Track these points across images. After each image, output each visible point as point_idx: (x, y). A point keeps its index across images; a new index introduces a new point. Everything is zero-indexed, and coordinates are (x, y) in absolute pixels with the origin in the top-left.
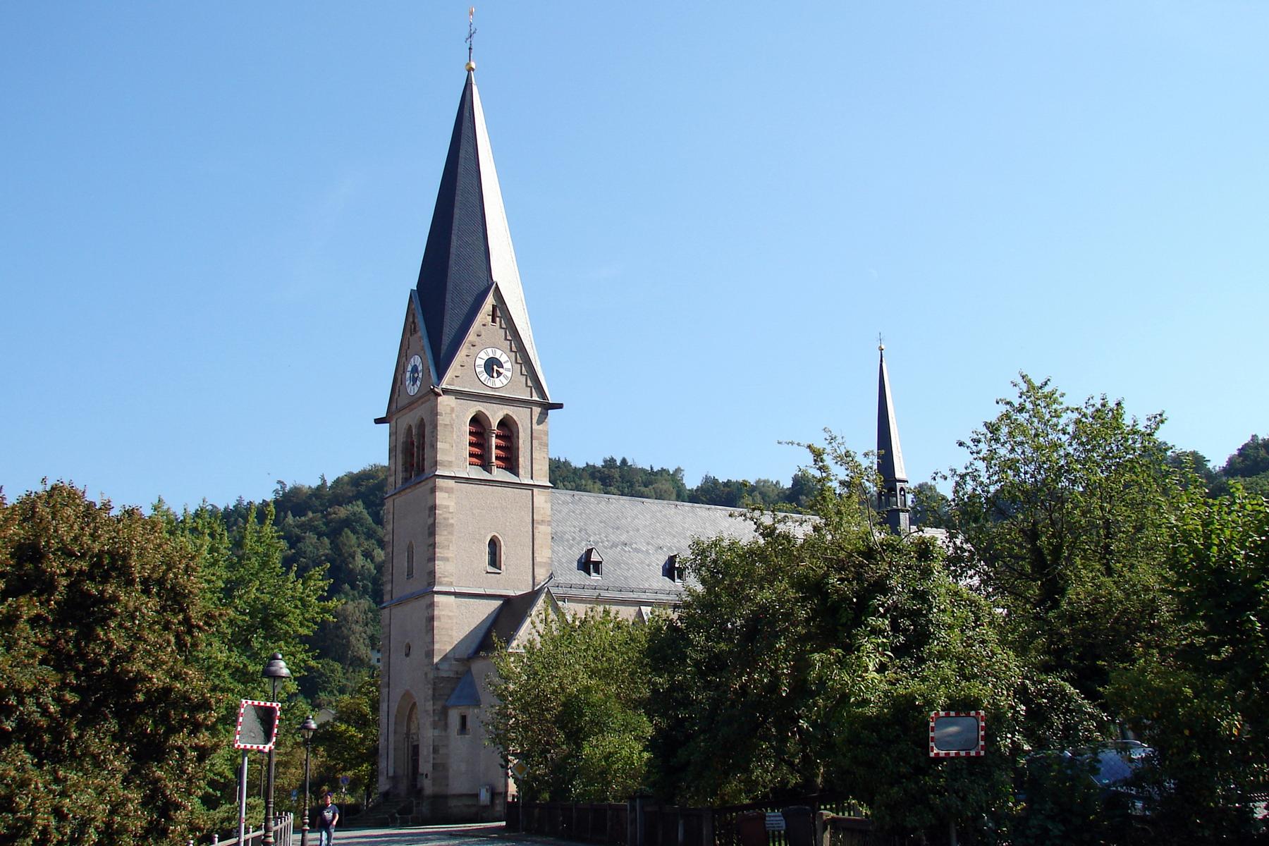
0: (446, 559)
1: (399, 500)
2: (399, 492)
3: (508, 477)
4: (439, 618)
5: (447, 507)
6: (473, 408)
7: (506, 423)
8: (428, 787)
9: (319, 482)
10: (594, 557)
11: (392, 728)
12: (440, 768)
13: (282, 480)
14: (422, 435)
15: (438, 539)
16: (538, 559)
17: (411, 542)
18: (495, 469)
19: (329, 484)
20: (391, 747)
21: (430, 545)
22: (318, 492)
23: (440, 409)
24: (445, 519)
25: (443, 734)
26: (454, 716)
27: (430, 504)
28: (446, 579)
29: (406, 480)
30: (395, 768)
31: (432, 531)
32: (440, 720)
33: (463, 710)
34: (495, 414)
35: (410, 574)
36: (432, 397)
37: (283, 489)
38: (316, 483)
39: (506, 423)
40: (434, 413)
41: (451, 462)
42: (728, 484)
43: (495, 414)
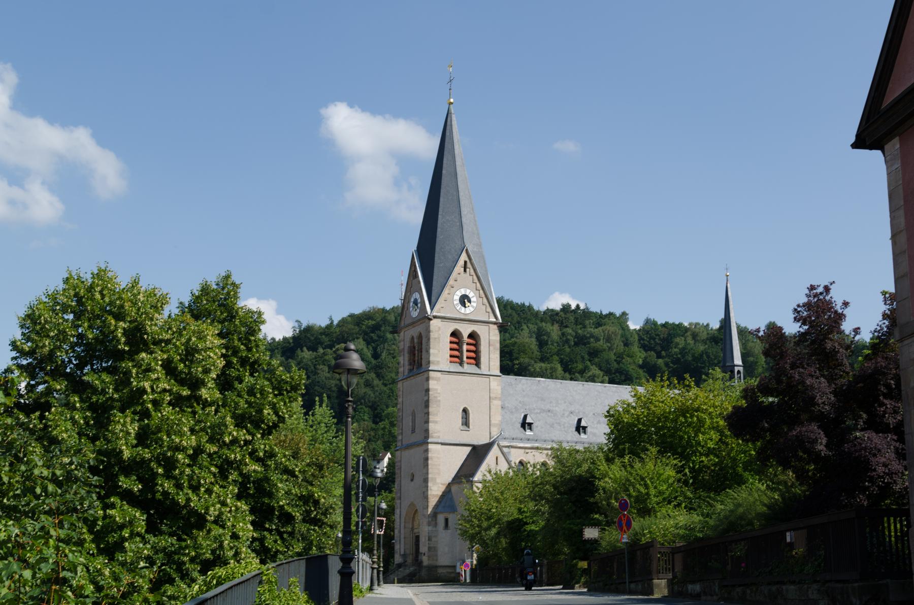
0: (436, 422)
1: (407, 383)
2: (406, 378)
3: (473, 369)
4: (432, 458)
5: (437, 390)
6: (453, 326)
7: (473, 335)
8: (425, 561)
9: (328, 322)
10: (529, 420)
11: (402, 525)
12: (432, 549)
13: (300, 320)
14: (421, 343)
15: (431, 410)
16: (493, 422)
17: (414, 410)
18: (465, 365)
19: (335, 323)
20: (402, 536)
21: (426, 413)
22: (327, 331)
23: (432, 328)
24: (435, 397)
25: (434, 529)
27: (425, 388)
28: (436, 434)
29: (410, 370)
30: (405, 550)
31: (427, 405)
32: (432, 520)
35: (413, 431)
36: (427, 321)
37: (300, 327)
38: (324, 323)
39: (473, 335)
40: (428, 331)
41: (438, 362)
42: (665, 325)
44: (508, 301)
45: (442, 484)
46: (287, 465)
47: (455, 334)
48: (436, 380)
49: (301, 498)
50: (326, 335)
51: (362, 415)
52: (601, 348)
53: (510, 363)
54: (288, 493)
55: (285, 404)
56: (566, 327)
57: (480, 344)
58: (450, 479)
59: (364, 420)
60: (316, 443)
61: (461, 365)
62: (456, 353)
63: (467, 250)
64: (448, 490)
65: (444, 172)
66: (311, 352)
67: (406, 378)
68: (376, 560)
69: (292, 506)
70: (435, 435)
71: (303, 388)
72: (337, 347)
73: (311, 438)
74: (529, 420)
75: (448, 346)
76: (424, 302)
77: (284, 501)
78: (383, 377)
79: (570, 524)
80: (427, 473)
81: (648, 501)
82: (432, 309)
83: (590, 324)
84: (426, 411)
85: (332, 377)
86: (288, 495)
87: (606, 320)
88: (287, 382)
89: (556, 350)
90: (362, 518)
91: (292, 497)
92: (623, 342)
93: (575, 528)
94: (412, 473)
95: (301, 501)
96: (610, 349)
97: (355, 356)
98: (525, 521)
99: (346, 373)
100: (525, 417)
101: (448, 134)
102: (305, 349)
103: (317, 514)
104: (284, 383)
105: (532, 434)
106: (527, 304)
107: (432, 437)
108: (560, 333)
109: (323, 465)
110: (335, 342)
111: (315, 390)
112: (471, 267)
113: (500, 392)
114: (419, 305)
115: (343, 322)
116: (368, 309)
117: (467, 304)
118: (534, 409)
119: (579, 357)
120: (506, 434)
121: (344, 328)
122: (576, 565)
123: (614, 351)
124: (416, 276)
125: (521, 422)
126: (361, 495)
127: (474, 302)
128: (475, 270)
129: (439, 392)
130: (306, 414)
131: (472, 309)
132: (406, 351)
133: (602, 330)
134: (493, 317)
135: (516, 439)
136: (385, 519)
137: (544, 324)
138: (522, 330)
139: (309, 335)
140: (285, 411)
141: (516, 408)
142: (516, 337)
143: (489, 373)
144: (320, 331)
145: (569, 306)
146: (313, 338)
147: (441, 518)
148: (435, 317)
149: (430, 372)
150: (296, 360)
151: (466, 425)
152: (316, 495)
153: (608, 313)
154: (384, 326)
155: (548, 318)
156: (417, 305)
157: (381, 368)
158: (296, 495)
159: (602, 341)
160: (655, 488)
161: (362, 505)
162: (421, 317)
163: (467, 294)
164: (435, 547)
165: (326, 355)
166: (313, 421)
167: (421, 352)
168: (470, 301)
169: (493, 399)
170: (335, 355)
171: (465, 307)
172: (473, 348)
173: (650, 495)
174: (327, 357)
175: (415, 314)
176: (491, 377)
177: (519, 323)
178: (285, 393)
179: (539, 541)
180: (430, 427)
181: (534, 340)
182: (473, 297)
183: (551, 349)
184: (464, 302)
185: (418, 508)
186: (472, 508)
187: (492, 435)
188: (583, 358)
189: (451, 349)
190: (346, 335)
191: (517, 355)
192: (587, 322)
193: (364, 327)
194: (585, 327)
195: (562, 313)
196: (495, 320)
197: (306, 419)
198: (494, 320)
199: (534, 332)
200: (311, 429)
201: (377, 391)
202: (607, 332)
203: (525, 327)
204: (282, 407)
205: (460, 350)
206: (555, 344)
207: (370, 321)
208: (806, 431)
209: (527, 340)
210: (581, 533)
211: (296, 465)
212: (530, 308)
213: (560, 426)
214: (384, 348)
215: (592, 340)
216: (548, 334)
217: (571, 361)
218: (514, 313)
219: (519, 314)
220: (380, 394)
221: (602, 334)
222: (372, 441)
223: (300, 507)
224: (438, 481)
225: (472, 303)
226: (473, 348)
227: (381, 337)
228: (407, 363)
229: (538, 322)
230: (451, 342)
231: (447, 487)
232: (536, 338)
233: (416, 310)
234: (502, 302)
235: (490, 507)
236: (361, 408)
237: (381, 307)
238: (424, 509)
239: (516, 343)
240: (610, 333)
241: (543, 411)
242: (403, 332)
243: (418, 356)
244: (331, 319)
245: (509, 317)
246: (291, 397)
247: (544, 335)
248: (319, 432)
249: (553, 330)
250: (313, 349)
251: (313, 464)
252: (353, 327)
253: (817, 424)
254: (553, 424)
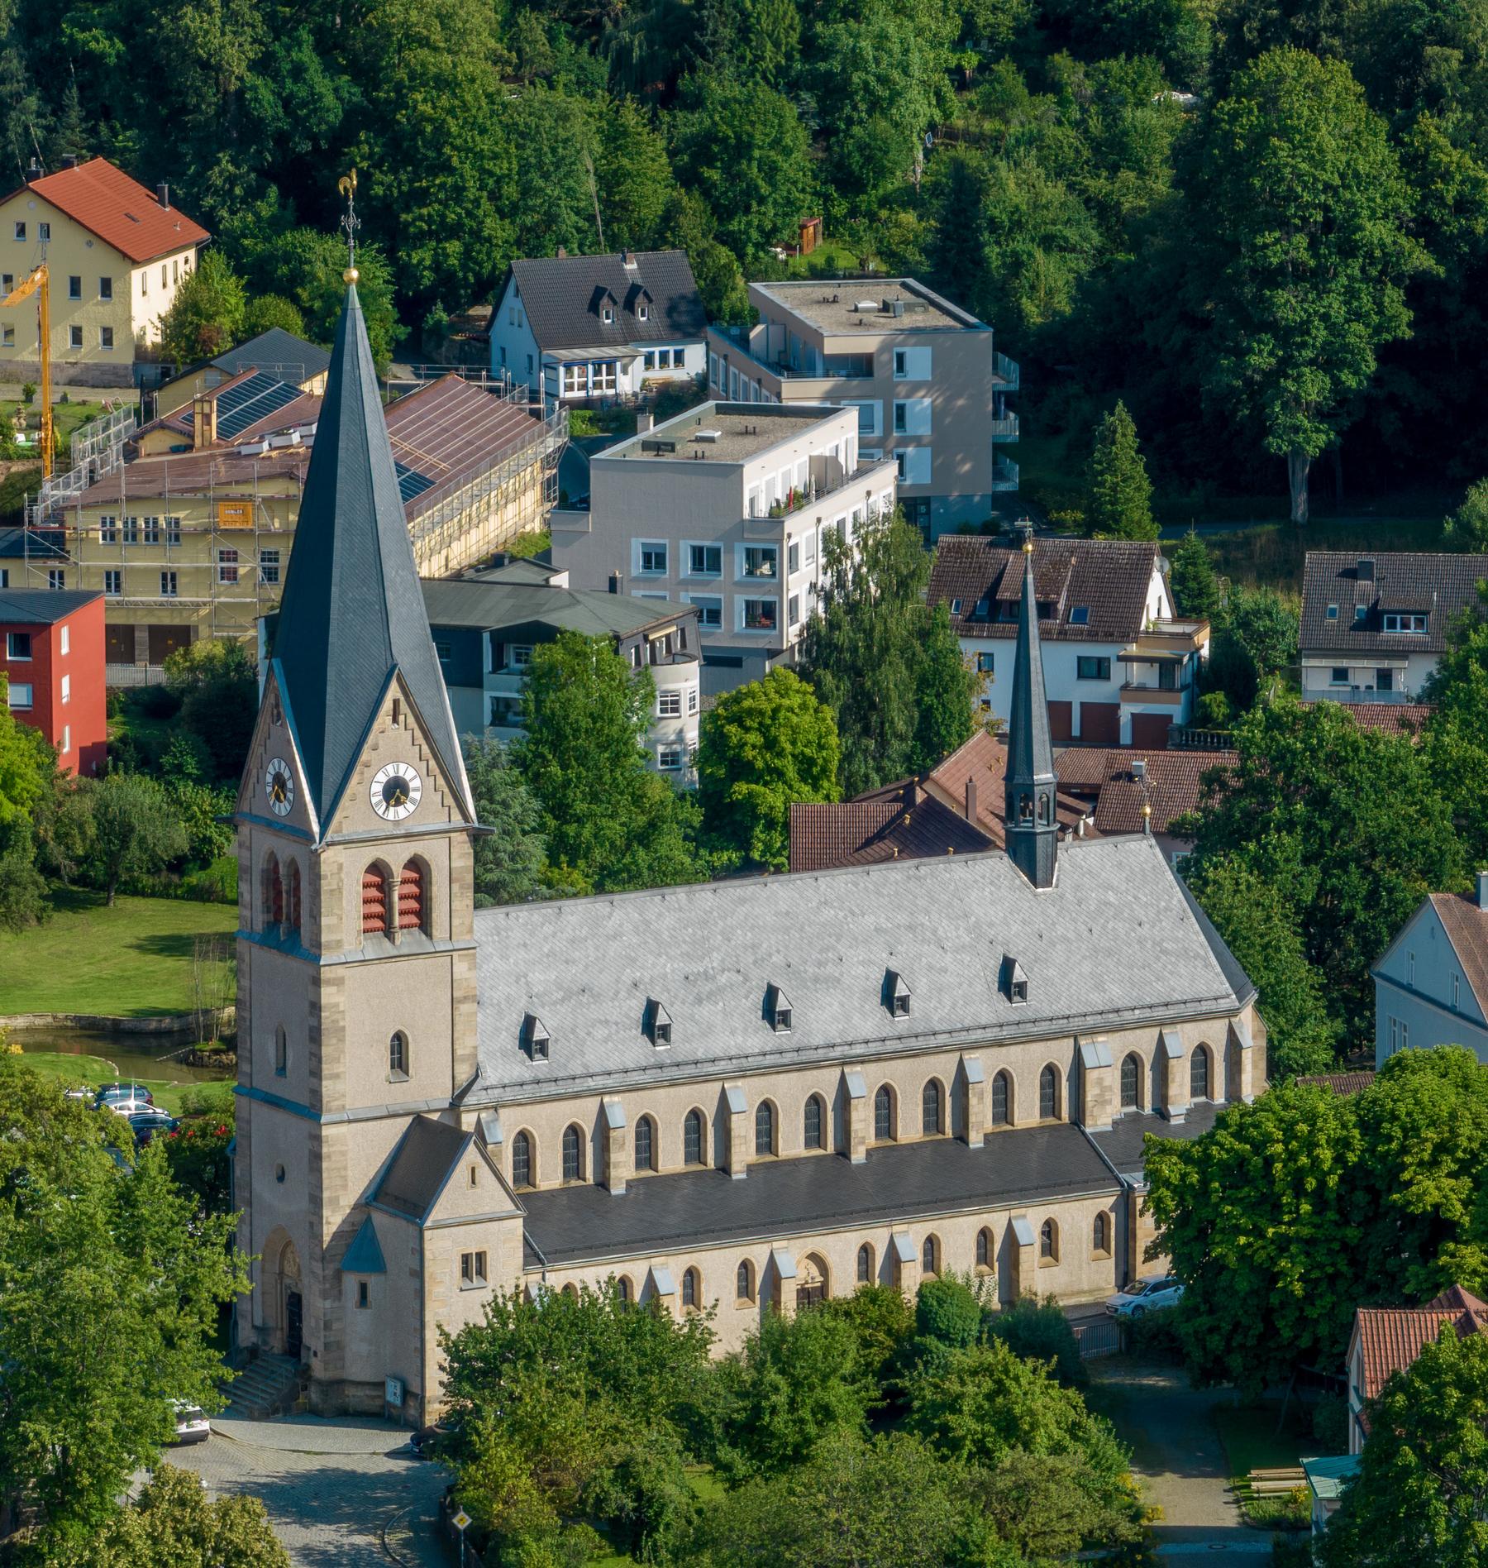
0: (337, 1076)
5: (337, 1005)
7: (417, 865)
12: (334, 1347)
15: (325, 1051)
16: (459, 1052)
25: (336, 1304)
26: (351, 1282)
31: (315, 1036)
33: (364, 1278)
34: (396, 857)
43: (396, 857)
47: (377, 868)
64: (362, 1217)
76: (301, 790)
84: (313, 1022)
112: (408, 711)
131: (403, 767)
151: (400, 1067)
198: (461, 824)
205: (385, 902)
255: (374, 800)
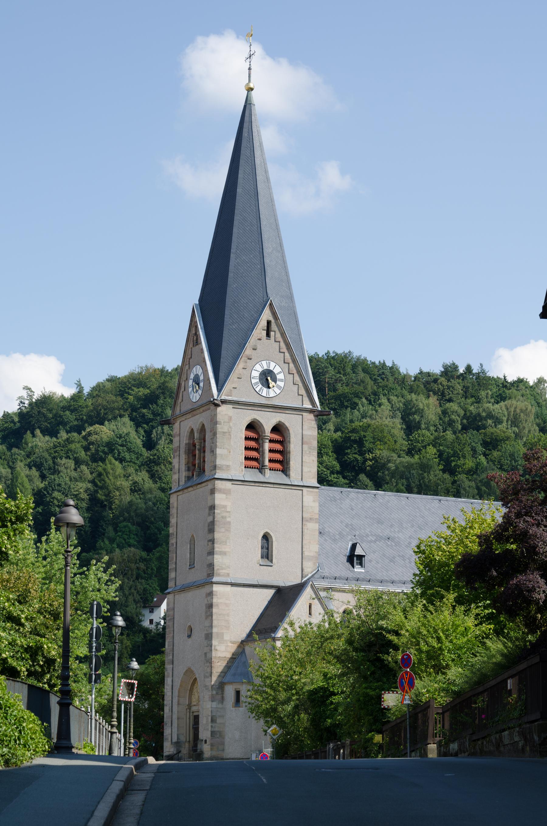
0: (224, 553)
1: (184, 497)
2: (183, 490)
3: (279, 477)
4: (217, 605)
5: (225, 507)
8: (206, 749)
10: (359, 551)
13: (29, 386)
14: (203, 440)
15: (217, 535)
16: (306, 553)
18: (267, 471)
19: (87, 390)
20: (175, 717)
23: (219, 418)
24: (222, 517)
25: (220, 706)
27: (210, 504)
28: (224, 571)
29: (189, 478)
30: (178, 735)
35: (192, 566)
36: (212, 407)
39: (278, 429)
40: (214, 422)
41: (228, 466)
44: (358, 359)
45: (233, 643)
46: (10, 612)
47: (252, 426)
48: (224, 493)
49: (28, 649)
50: (72, 411)
51: (126, 537)
52: (503, 434)
53: (359, 458)
54: (12, 644)
55: (9, 537)
56: (450, 400)
57: (289, 442)
58: (244, 636)
59: (130, 546)
60: (50, 582)
61: (261, 472)
62: (254, 454)
63: (271, 305)
64: (241, 650)
65: (239, 190)
66: (47, 438)
67: (183, 490)
68: (116, 723)
69: (17, 659)
70: (222, 572)
71: (31, 518)
72: (88, 430)
73: (44, 575)
74: (359, 551)
75: (243, 443)
76: (209, 379)
77: (7, 653)
78: (160, 478)
79: (366, 688)
80: (211, 626)
81: (441, 657)
82: (219, 390)
83: (487, 397)
84: (210, 537)
85: (81, 478)
86: (12, 646)
87: (513, 390)
88: (11, 512)
89: (432, 437)
90: (96, 671)
91: (17, 649)
92: (538, 425)
93: (372, 693)
94: (190, 627)
95: (27, 653)
96: (518, 436)
97: (74, 511)
98: (331, 690)
99: (66, 526)
100: (354, 546)
101: (245, 134)
102: (38, 432)
103: (51, 677)
104: (8, 513)
105: (363, 571)
106: (389, 364)
107: (219, 575)
108: (439, 410)
109: (59, 613)
110: (86, 421)
111: (53, 498)
113: (317, 510)
114: (201, 384)
115: (98, 389)
116: (137, 370)
117: (272, 384)
118: (367, 535)
119: (468, 449)
120: (326, 572)
121: (100, 400)
122: (372, 738)
123: (525, 439)
124: (197, 342)
125: (348, 554)
126: (94, 645)
127: (281, 380)
128: (283, 334)
129: (228, 510)
130: (38, 541)
132: (183, 450)
133: (506, 406)
134: (309, 403)
135: (340, 578)
136: (136, 682)
137: (414, 396)
138: (380, 405)
139: (44, 411)
140: (9, 546)
141: (340, 534)
142: (371, 417)
143: (301, 484)
144: (62, 404)
145: (455, 367)
146: (50, 416)
147: (230, 691)
148: (224, 402)
149: (217, 482)
150: (24, 449)
151: (268, 558)
152: (45, 646)
153: (516, 379)
154: (162, 398)
155: (422, 386)
156: (198, 384)
157: (158, 464)
158: (22, 646)
159: (504, 424)
160: (451, 641)
161: (95, 655)
162: (205, 401)
163: (271, 368)
164: (220, 732)
165: (72, 442)
166: (46, 551)
167: (204, 452)
168: (275, 380)
169: (307, 521)
170: (85, 443)
171: (269, 387)
172: (278, 447)
173: (444, 650)
174: (73, 446)
175: (195, 397)
176: (304, 489)
177: (375, 394)
178: (9, 524)
179: (340, 714)
180: (215, 561)
181: (398, 421)
182: (280, 373)
183: (423, 436)
184: (267, 380)
185: (197, 676)
186: (266, 675)
187: (305, 573)
188: (474, 450)
189: (247, 448)
190: (102, 411)
191: (371, 446)
192: (483, 393)
193: (131, 397)
194: (478, 401)
195: (443, 379)
196: (310, 407)
197: (37, 548)
199: (398, 409)
200: (45, 563)
201: (150, 500)
202: (512, 410)
203: (384, 400)
204: (6, 542)
206: (432, 428)
207: (141, 389)
208: (525, 580)
209: (387, 421)
210: (379, 699)
211: (22, 611)
212: (393, 370)
213: (404, 560)
214: (163, 433)
215: (490, 422)
216: (420, 412)
217: (455, 454)
218: (368, 379)
219: (375, 380)
220: (154, 504)
221: (506, 413)
222: (142, 578)
223: (26, 660)
224: (227, 637)
225: (278, 383)
226: (278, 447)
227: (159, 415)
228: (183, 467)
229: (405, 392)
230: (247, 439)
231: (239, 647)
232: (402, 418)
233: (197, 391)
234: (350, 361)
235: (291, 672)
236: (125, 527)
237: (158, 366)
238: (205, 677)
239: (369, 426)
240: (518, 411)
241: (379, 538)
242: (178, 422)
243: (200, 458)
244: (79, 385)
245: (359, 385)
246: (17, 529)
247: (414, 413)
248: (56, 567)
249: (428, 406)
250: (52, 432)
251: (46, 611)
252: (114, 398)
253: (540, 573)
254: (394, 558)
255: (254, 381)
